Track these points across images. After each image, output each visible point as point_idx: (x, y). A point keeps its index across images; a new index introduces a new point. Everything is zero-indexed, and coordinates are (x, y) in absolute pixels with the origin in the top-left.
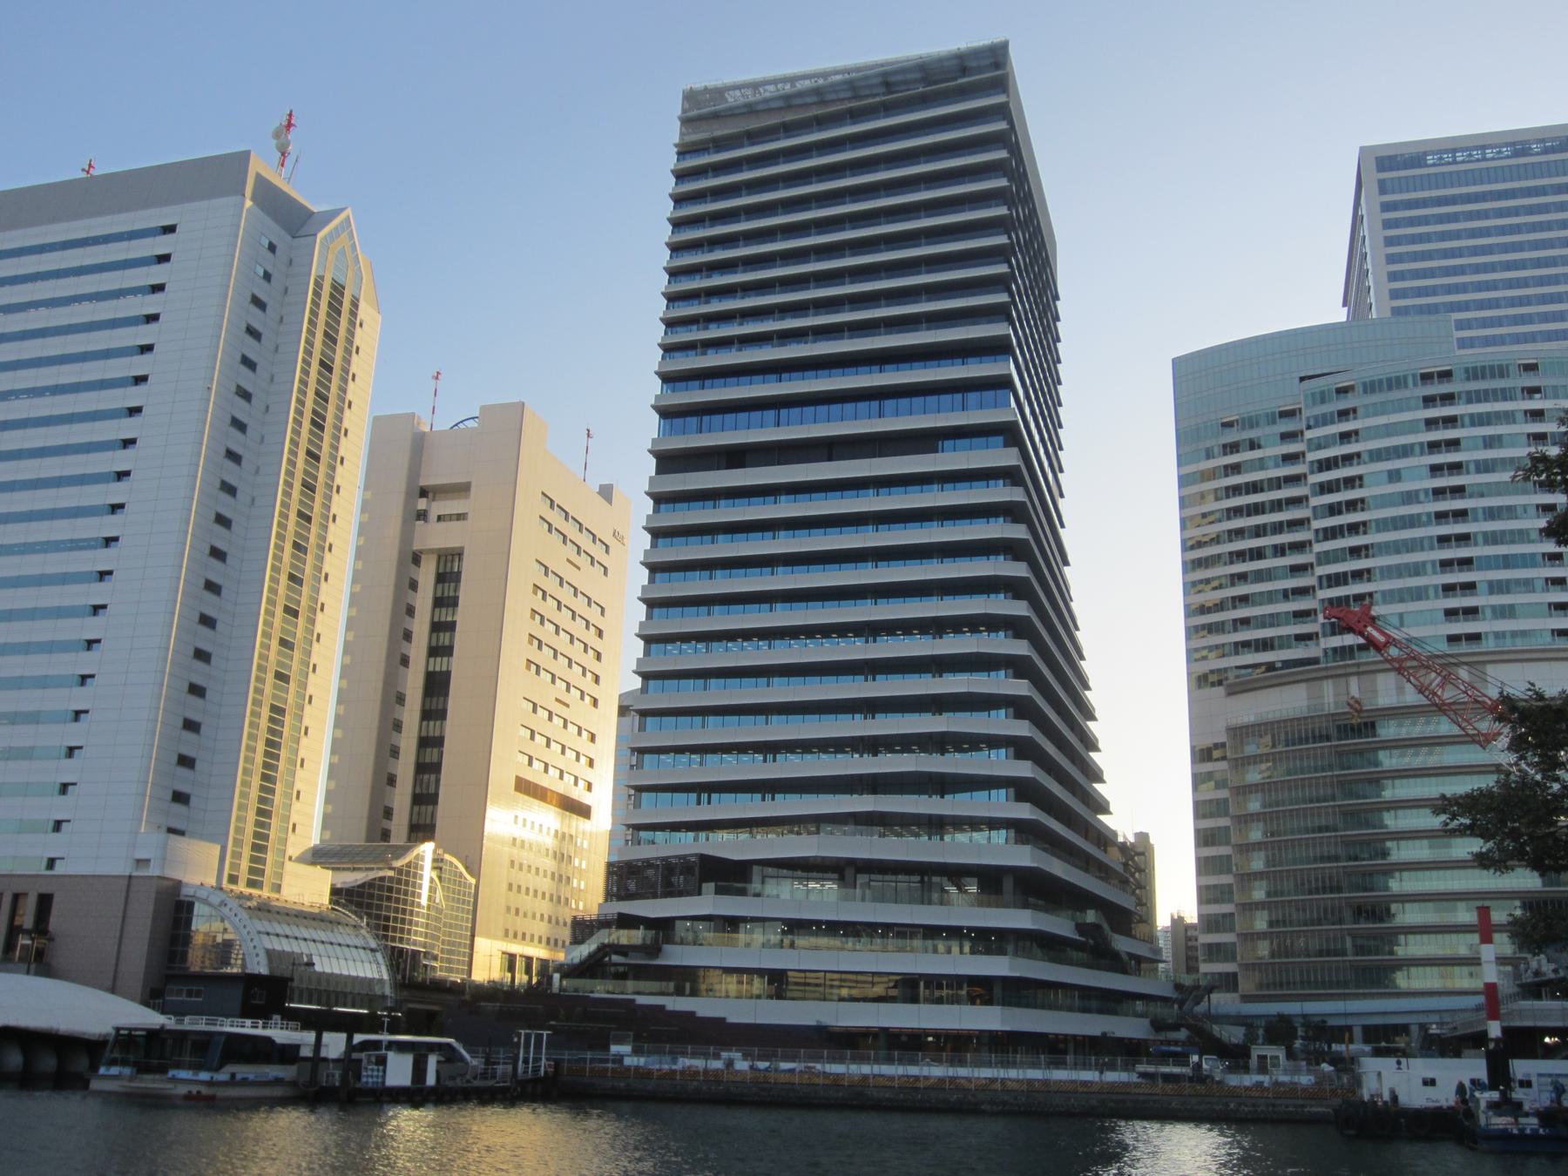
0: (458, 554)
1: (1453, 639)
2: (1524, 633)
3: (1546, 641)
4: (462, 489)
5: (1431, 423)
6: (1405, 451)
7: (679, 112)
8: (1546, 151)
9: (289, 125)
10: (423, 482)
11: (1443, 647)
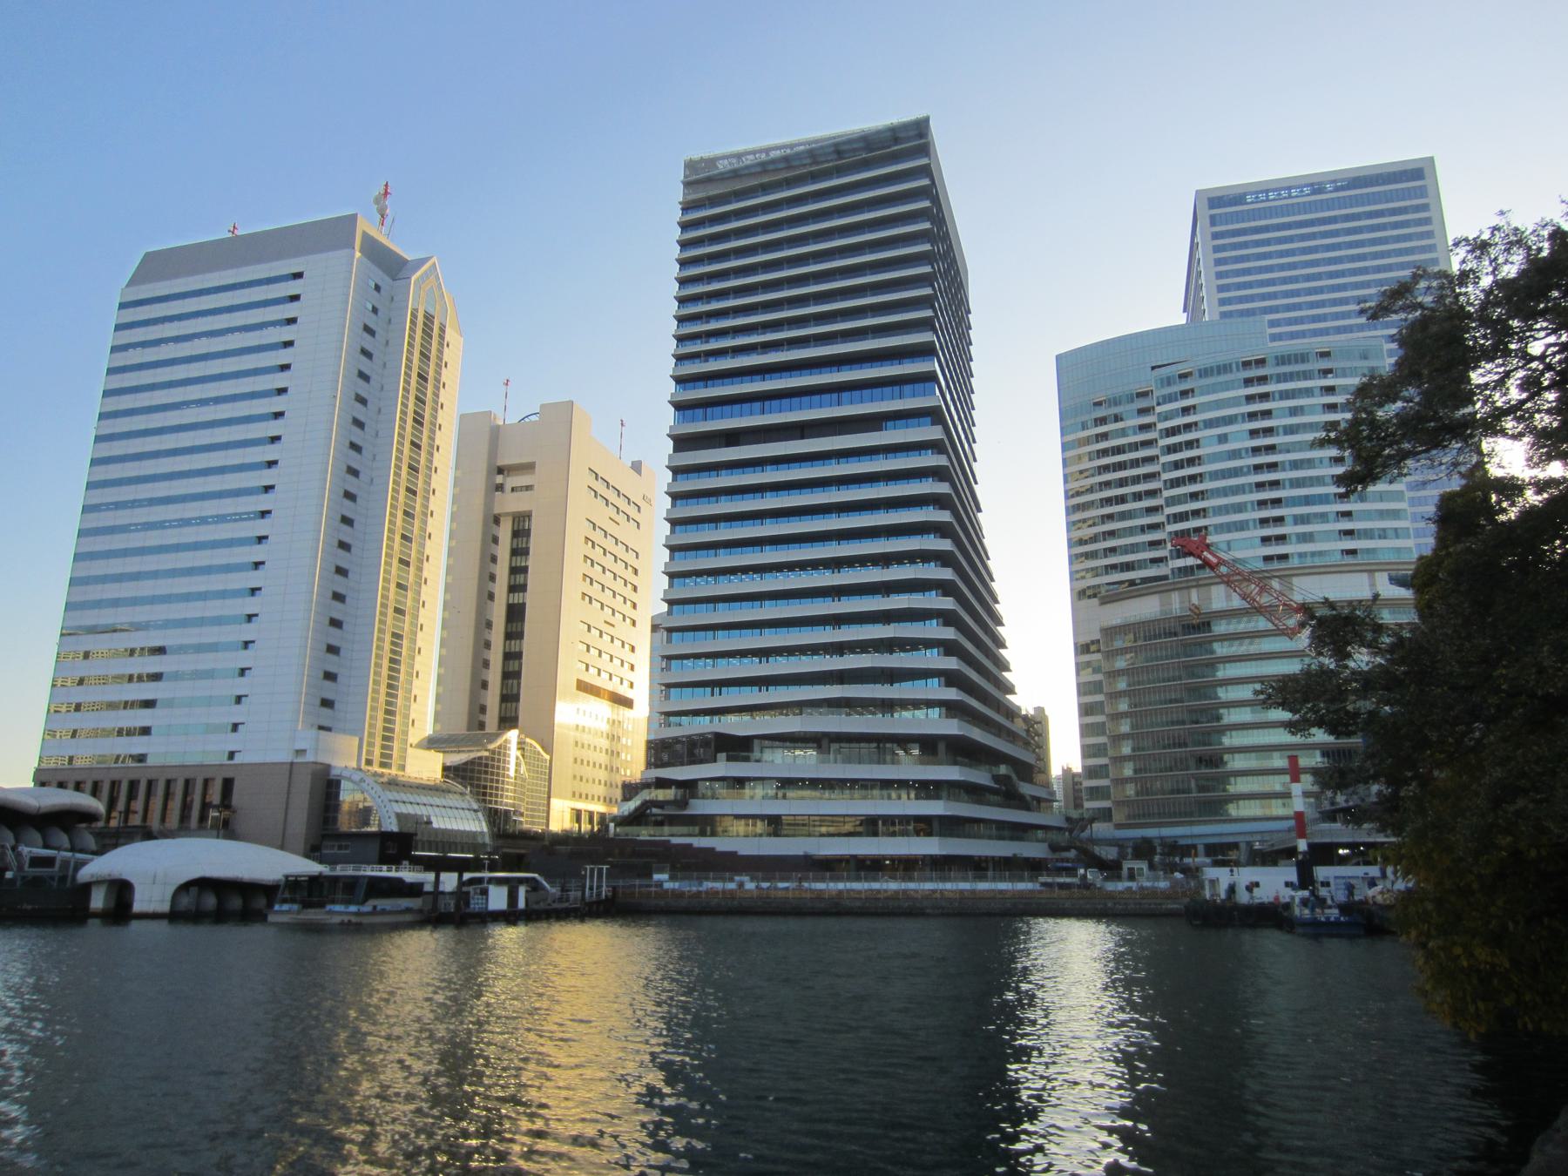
1: (1267, 559)
2: (1321, 553)
3: (1337, 558)
4: (529, 467)
6: (1230, 420)
8: (1337, 189)
9: (386, 193)
10: (500, 463)
11: (1261, 565)
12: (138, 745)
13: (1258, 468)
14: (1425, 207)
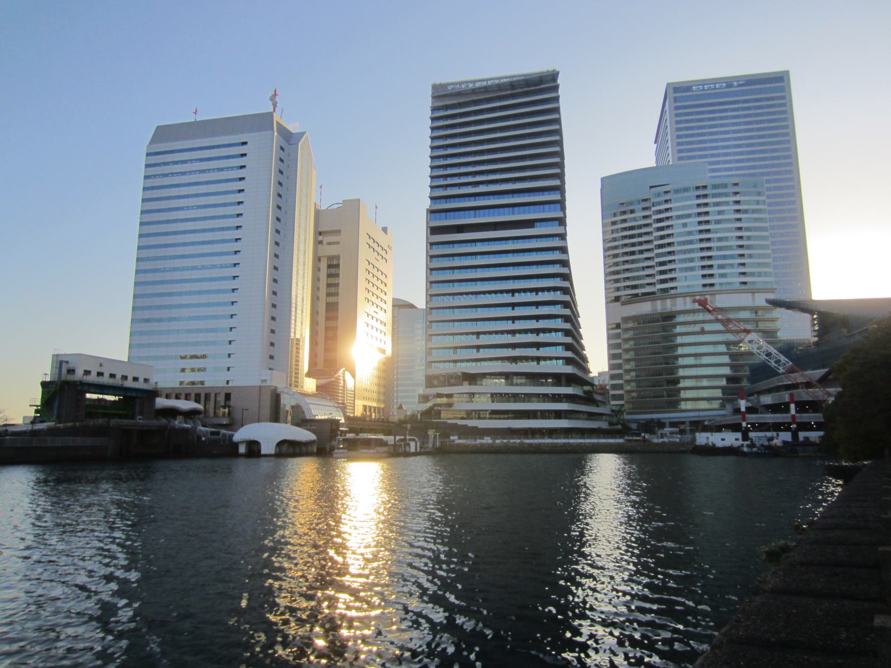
0: (338, 257)
1: (704, 285)
2: (730, 283)
3: (738, 286)
4: (338, 232)
5: (699, 205)
6: (689, 216)
7: (431, 93)
8: (739, 85)
9: (275, 95)
10: (320, 230)
11: (701, 289)
12: (197, 377)
13: (701, 240)
14: (783, 98)
